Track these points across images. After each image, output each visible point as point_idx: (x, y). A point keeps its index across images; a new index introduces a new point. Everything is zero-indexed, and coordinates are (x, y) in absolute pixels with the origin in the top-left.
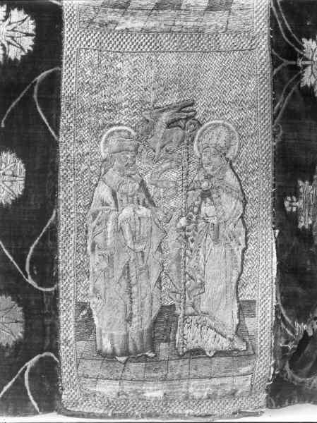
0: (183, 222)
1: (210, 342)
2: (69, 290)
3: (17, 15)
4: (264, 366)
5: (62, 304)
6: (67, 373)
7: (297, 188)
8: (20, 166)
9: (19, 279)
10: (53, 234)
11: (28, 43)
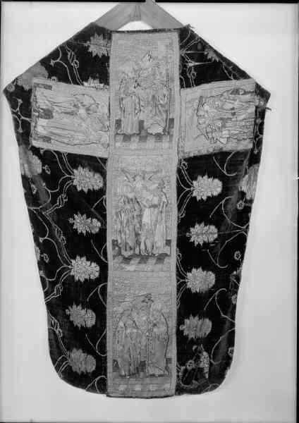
0: (147, 334)
1: (157, 372)
2: (110, 356)
4: (174, 381)
5: (108, 360)
6: (109, 382)
7: (190, 230)
8: (94, 314)
10: (105, 337)
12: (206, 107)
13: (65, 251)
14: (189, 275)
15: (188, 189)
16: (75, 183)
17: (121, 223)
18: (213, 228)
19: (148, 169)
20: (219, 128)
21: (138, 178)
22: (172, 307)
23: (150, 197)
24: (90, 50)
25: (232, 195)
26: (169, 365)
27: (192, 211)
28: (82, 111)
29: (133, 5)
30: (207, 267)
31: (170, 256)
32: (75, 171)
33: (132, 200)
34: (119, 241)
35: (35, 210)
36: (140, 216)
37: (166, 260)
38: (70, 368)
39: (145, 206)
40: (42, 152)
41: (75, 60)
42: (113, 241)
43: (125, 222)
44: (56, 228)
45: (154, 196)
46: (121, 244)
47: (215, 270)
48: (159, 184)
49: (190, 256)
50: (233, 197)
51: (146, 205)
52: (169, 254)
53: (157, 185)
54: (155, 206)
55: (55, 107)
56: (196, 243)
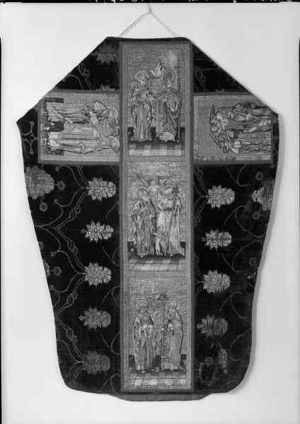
2: (125, 353)
3: (105, 269)
7: (201, 321)
9: (109, 350)
11: (109, 278)
12: (219, 117)
13: (77, 260)
14: (206, 277)
15: (203, 196)
16: (90, 193)
17: (137, 225)
18: (228, 236)
19: (163, 174)
20: (231, 138)
21: (153, 182)
22: (188, 309)
23: (165, 201)
24: (98, 59)
25: (244, 204)
26: (184, 361)
27: (206, 219)
28: (94, 120)
29: (145, 5)
30: (222, 270)
31: (185, 256)
32: (90, 183)
33: (147, 203)
34: (135, 243)
35: (46, 227)
36: (155, 218)
37: (181, 261)
38: (85, 373)
39: (160, 210)
40: (57, 169)
41: (85, 70)
42: (129, 243)
43: (141, 224)
44: (68, 241)
45: (169, 199)
46: (136, 245)
47: (230, 273)
48: (174, 189)
49: (205, 260)
50: (247, 208)
51: (161, 207)
52: (183, 254)
53: (171, 190)
54: (168, 209)
55: (66, 119)
56: (212, 247)
